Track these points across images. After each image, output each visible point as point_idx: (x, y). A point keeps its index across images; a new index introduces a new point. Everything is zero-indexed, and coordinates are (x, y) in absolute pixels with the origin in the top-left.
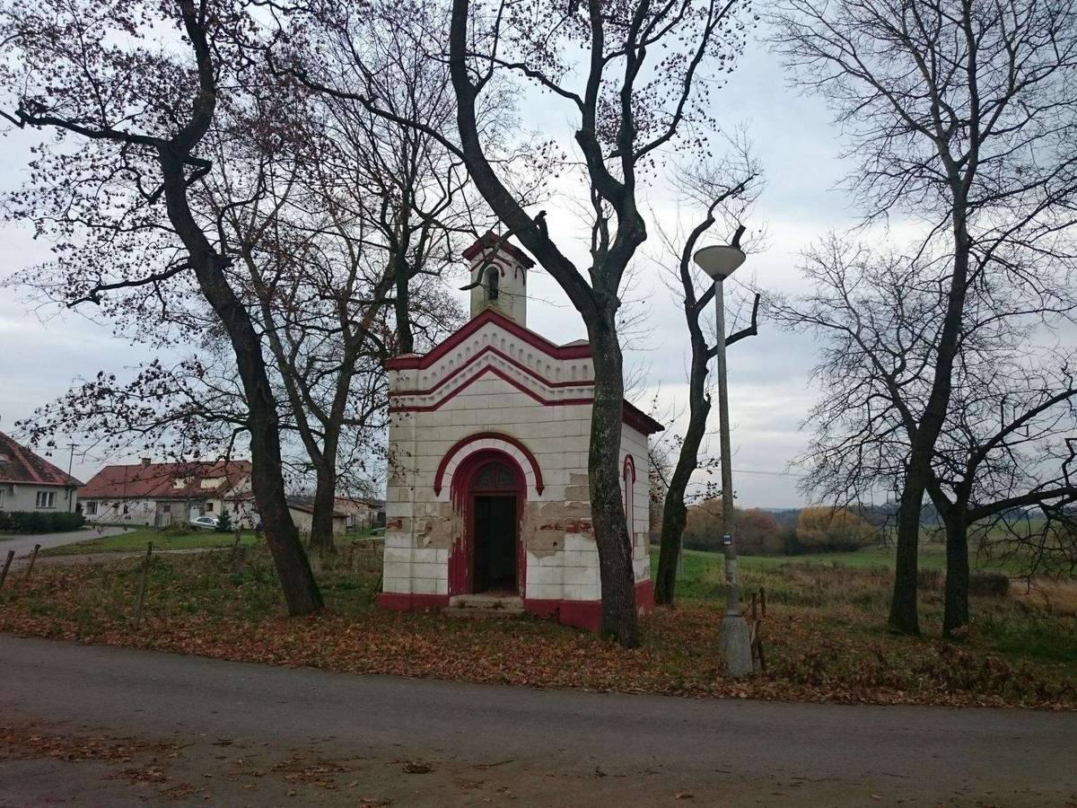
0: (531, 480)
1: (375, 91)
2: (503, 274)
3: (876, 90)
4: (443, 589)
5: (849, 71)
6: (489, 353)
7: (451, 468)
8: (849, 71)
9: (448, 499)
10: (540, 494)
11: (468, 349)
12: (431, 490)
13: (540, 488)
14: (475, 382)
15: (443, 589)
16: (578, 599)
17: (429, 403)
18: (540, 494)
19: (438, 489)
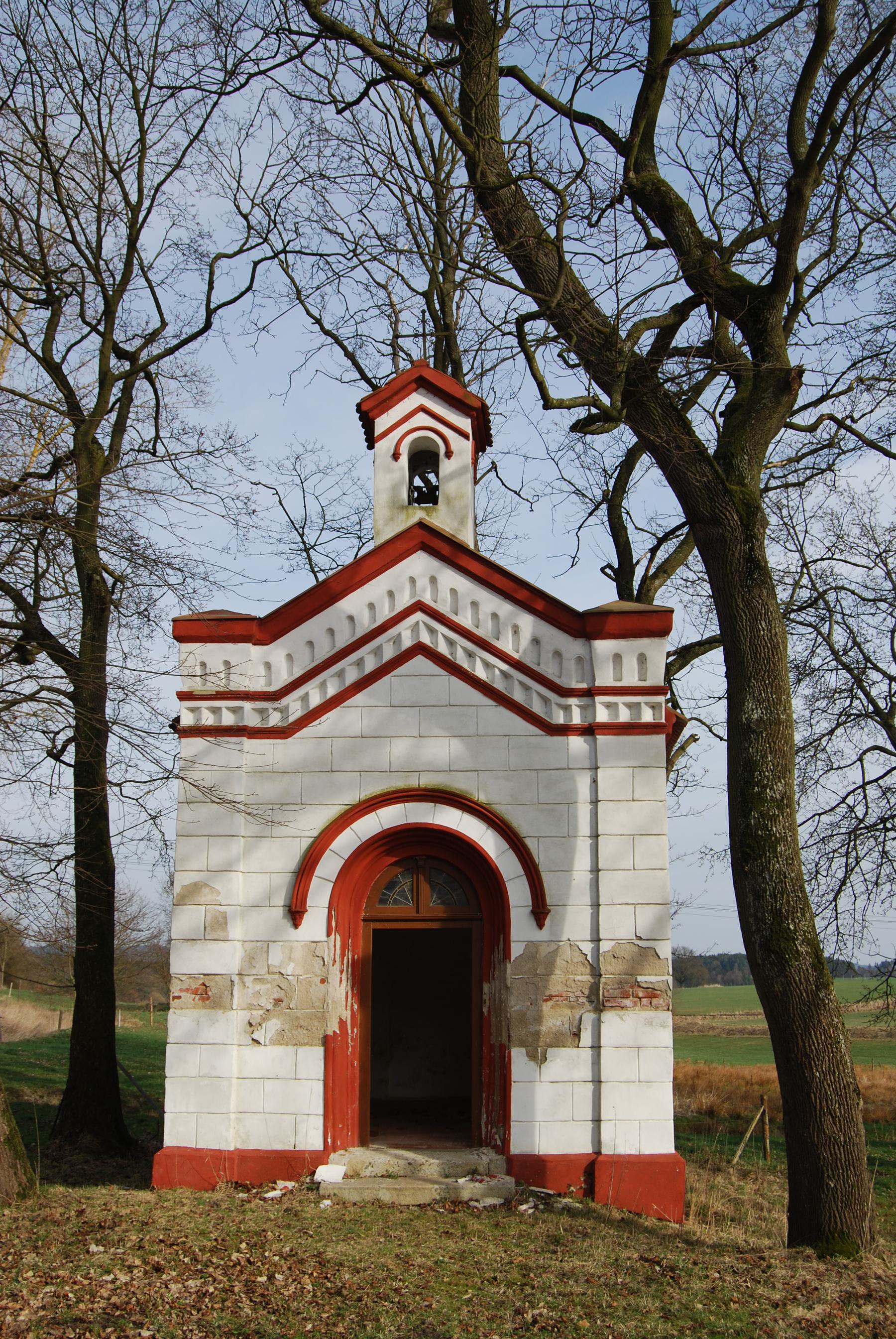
0: (518, 894)
1: (90, 9)
2: (449, 454)
3: (488, 367)
4: (312, 1138)
5: (578, 79)
6: (419, 616)
7: (329, 866)
8: (578, 79)
9: (321, 934)
10: (540, 925)
11: (331, 631)
12: (277, 912)
13: (540, 911)
14: (386, 679)
15: (312, 1138)
16: (633, 1151)
17: (275, 720)
18: (540, 925)
19: (295, 913)
